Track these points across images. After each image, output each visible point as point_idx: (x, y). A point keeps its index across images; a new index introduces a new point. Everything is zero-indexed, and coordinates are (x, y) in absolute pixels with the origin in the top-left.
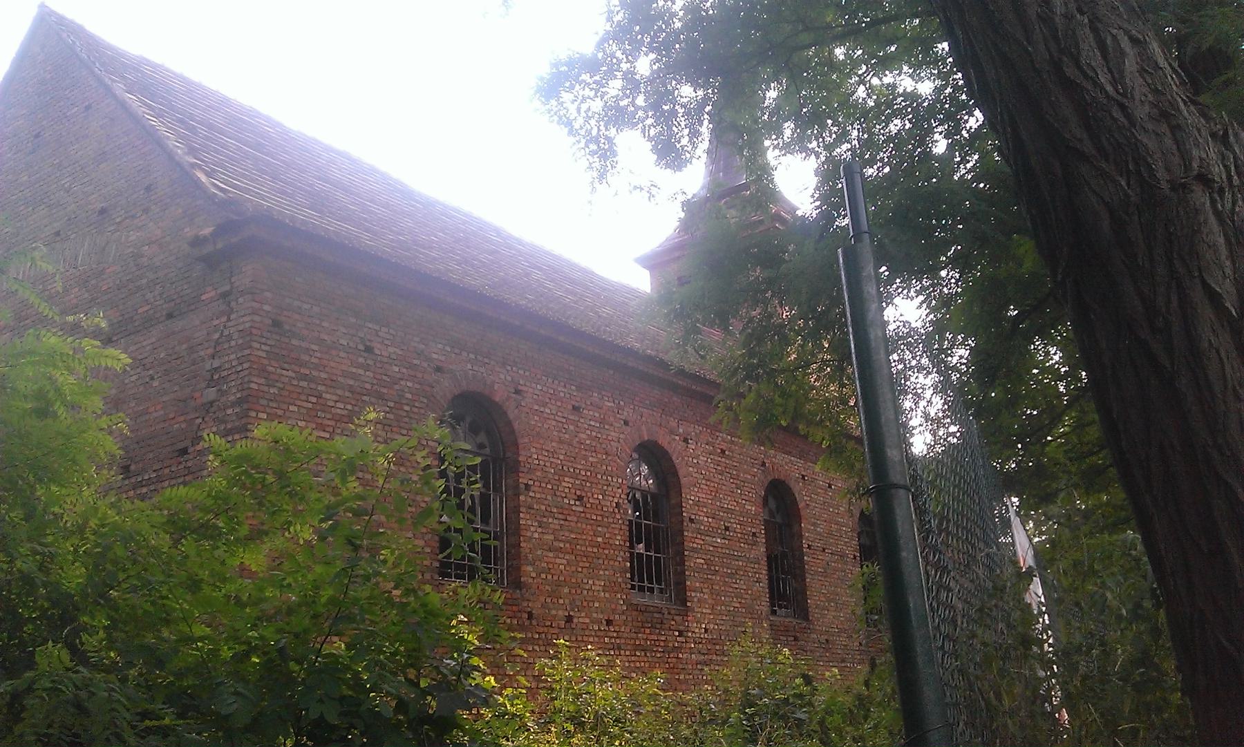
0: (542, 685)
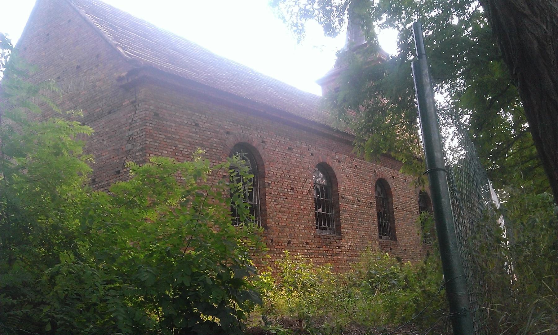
0: (278, 271)
